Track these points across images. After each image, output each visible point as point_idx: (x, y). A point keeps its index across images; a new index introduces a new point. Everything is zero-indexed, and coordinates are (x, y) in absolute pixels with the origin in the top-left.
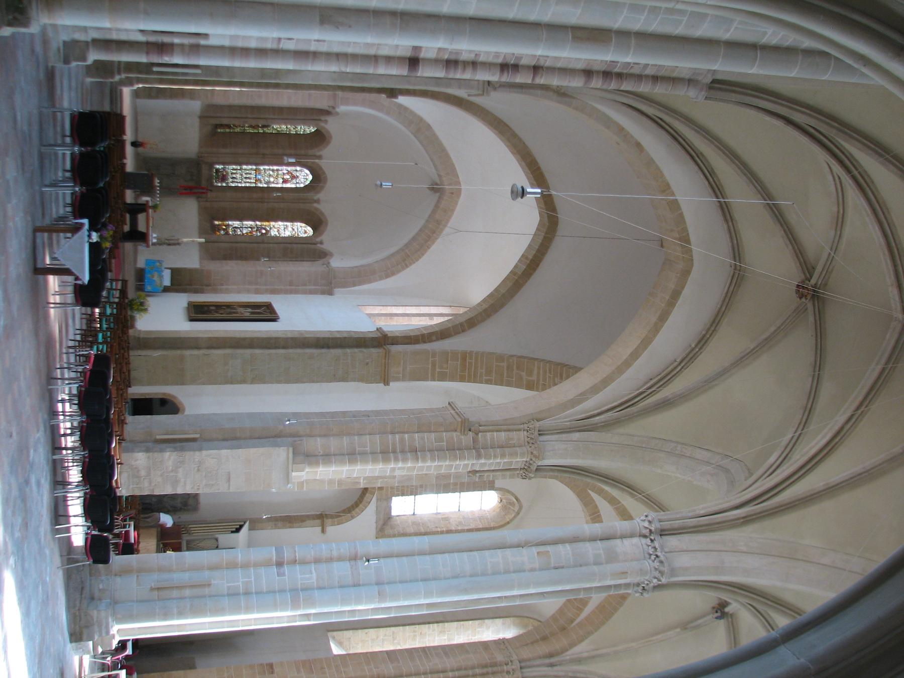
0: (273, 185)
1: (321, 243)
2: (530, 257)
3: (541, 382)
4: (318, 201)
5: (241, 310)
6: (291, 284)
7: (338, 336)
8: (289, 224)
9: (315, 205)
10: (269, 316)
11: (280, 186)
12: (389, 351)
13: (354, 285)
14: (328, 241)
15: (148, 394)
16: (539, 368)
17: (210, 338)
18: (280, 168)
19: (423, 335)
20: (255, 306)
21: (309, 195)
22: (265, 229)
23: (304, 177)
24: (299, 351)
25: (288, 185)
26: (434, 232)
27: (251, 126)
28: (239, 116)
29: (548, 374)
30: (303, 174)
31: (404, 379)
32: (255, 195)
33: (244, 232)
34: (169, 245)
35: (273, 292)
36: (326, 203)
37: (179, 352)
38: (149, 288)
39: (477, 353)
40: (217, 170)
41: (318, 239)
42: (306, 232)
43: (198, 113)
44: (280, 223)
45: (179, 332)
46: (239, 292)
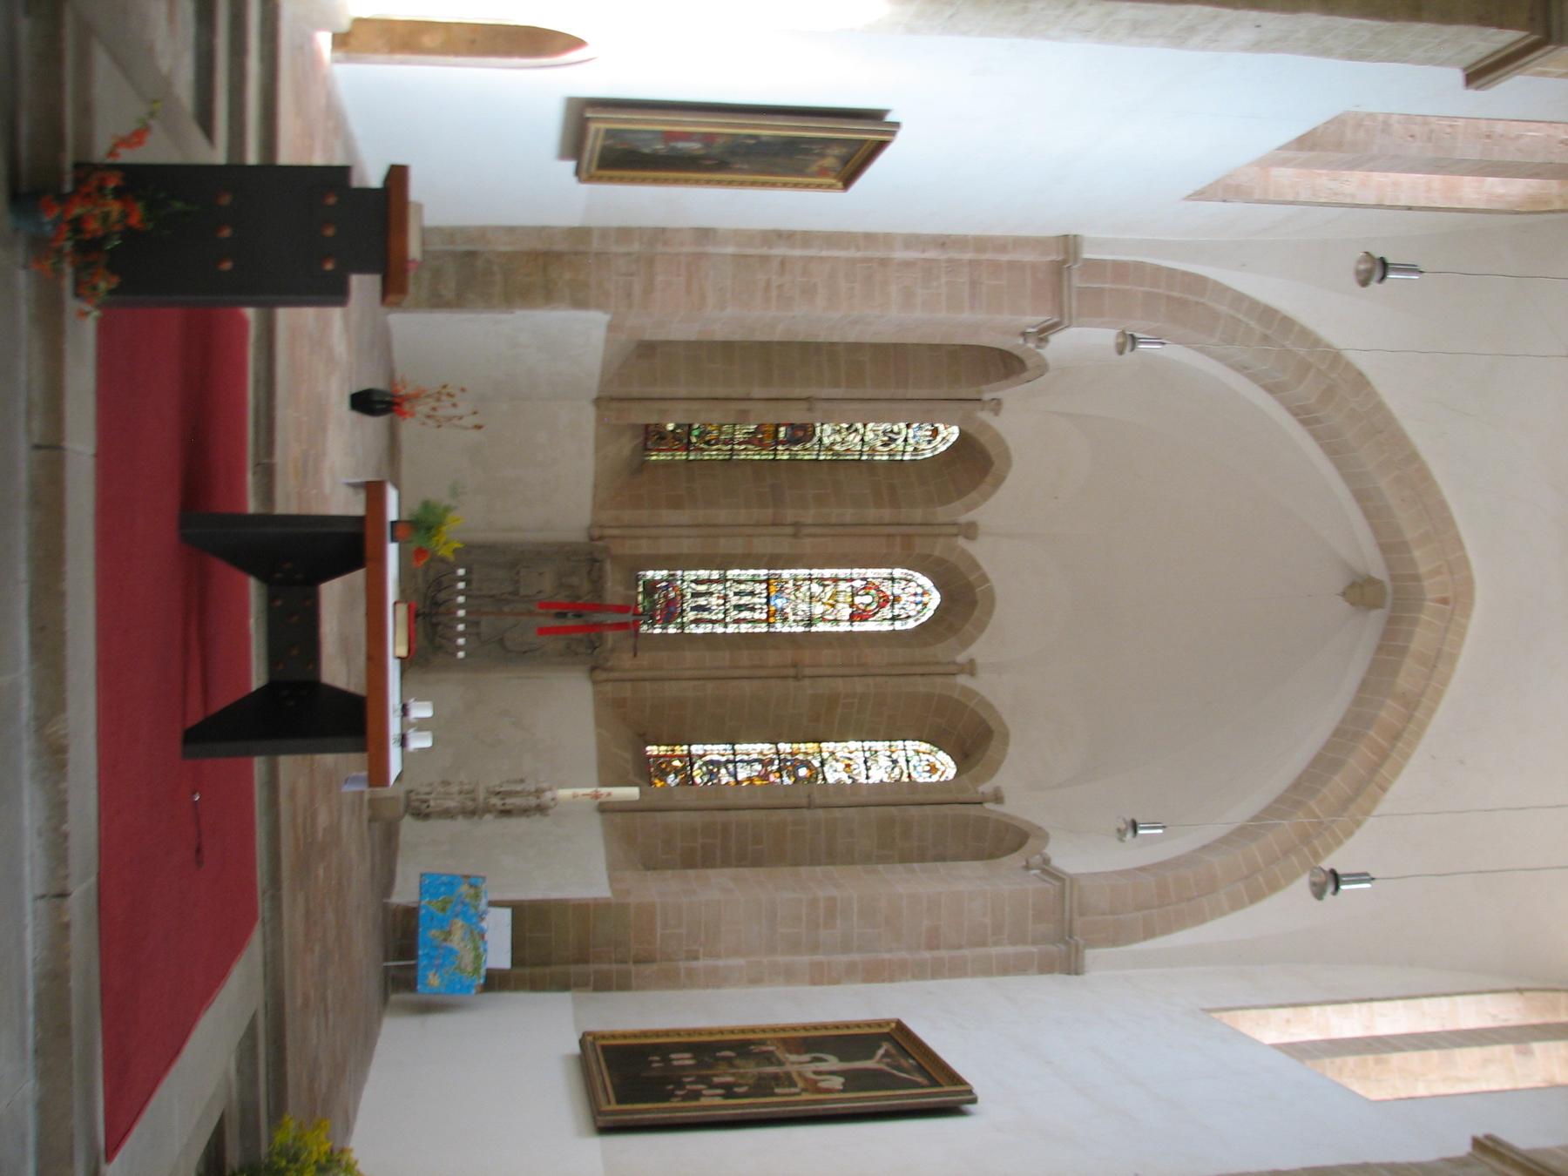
0: (821, 627)
1: (998, 798)
4: (970, 668)
5: (796, 1063)
8: (880, 746)
9: (962, 680)
11: (844, 627)
13: (1149, 933)
14: (1017, 788)
18: (843, 573)
21: (939, 651)
22: (807, 764)
25: (869, 626)
26: (1397, 737)
28: (721, 391)
30: (913, 588)
32: (772, 657)
33: (743, 774)
34: (506, 813)
36: (998, 668)
38: (432, 981)
40: (651, 587)
42: (933, 769)
43: (593, 386)
44: (853, 745)
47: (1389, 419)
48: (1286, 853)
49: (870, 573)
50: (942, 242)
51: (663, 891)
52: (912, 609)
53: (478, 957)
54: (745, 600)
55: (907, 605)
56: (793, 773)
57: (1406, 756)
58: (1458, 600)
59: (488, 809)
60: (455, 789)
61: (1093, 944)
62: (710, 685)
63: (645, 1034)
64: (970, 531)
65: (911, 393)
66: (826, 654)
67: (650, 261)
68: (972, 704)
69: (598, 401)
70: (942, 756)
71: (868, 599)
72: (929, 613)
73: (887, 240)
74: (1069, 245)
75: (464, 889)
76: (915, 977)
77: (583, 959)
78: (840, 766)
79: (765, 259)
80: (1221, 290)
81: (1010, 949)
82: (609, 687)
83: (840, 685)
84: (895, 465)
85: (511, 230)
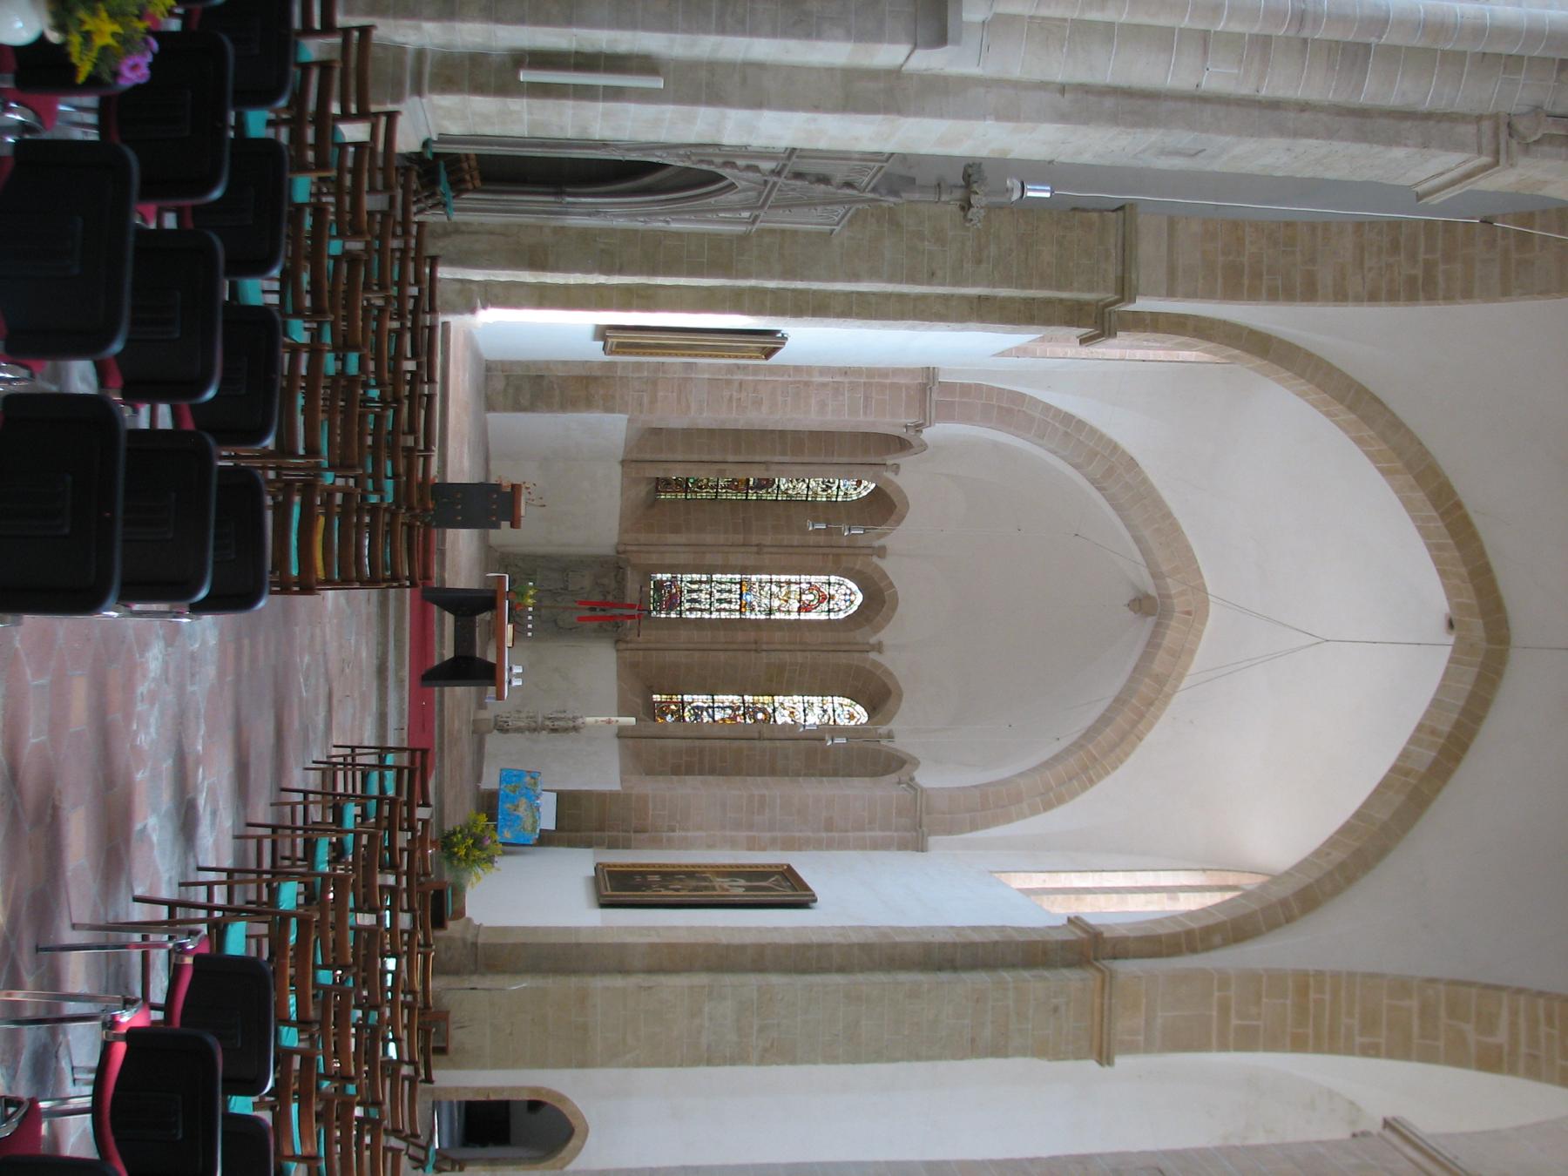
0: (778, 616)
1: (890, 736)
2: (1445, 728)
3: (1523, 1049)
4: (878, 647)
5: (725, 882)
6: (829, 826)
7: (977, 938)
8: (816, 700)
9: (873, 655)
10: (787, 894)
11: (794, 616)
12: (1112, 975)
14: (903, 732)
15: (495, 1090)
16: (1514, 1013)
17: (653, 947)
18: (793, 578)
19: (1189, 934)
20: (754, 874)
21: (858, 635)
22: (764, 711)
23: (846, 597)
24: (881, 977)
25: (812, 616)
27: (733, 485)
29: (1543, 1029)
30: (843, 590)
31: (1148, 1048)
32: (740, 636)
34: (554, 730)
35: (789, 845)
36: (898, 649)
37: (573, 981)
39: (1336, 975)
40: (659, 585)
41: (883, 729)
42: (852, 717)
43: (620, 455)
44: (796, 698)
45: (577, 930)
46: (711, 846)
47: (1151, 490)
48: (1070, 779)
49: (813, 579)
50: (845, 372)
51: (654, 788)
52: (843, 605)
53: (535, 822)
54: (725, 596)
55: (839, 601)
56: (754, 717)
57: (1157, 718)
58: (1197, 614)
59: (543, 729)
60: (523, 715)
61: (937, 833)
62: (697, 655)
63: (634, 865)
64: (881, 552)
65: (835, 460)
66: (778, 635)
67: (655, 383)
68: (879, 673)
69: (623, 462)
70: (859, 708)
71: (811, 597)
72: (855, 608)
73: (809, 370)
74: (930, 373)
75: (527, 779)
76: (815, 848)
77: (601, 829)
78: (786, 713)
79: (729, 382)
80: (1035, 402)
81: (879, 834)
82: (627, 654)
83: (787, 657)
84: (830, 503)
85: (565, 363)
